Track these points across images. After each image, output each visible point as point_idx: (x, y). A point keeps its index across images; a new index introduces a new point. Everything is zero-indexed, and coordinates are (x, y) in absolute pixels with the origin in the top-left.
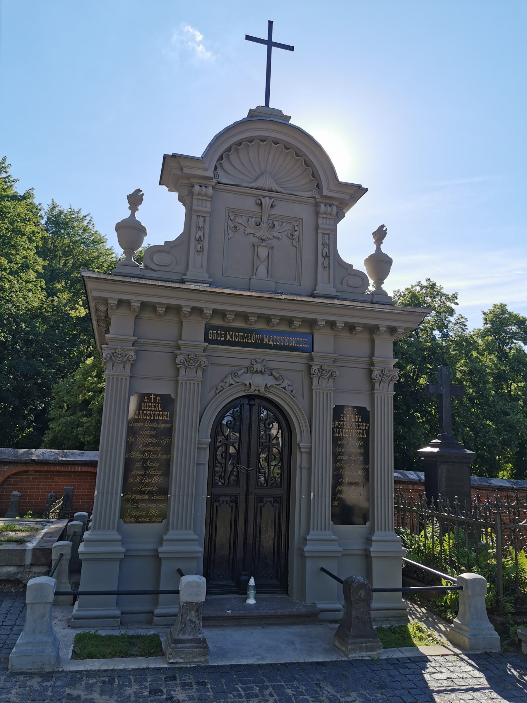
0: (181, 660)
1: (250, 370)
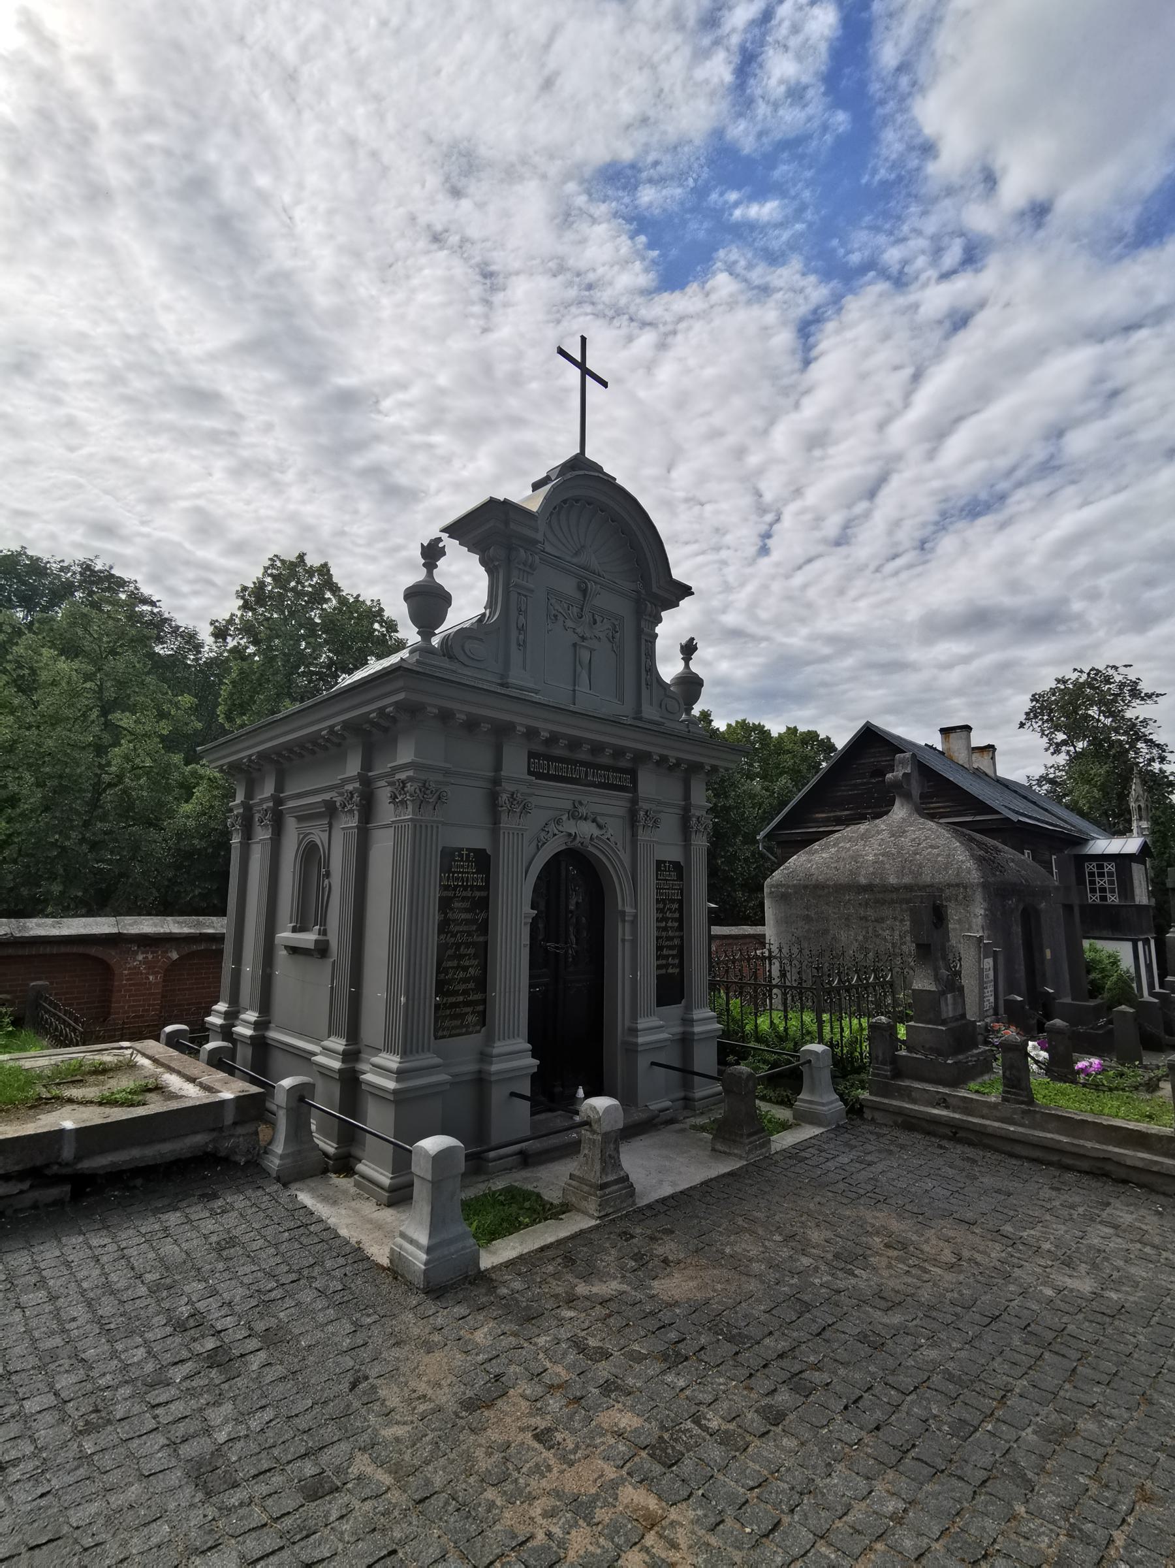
0: (611, 1210)
1: (574, 815)
